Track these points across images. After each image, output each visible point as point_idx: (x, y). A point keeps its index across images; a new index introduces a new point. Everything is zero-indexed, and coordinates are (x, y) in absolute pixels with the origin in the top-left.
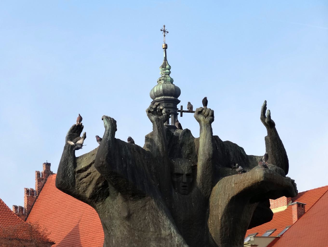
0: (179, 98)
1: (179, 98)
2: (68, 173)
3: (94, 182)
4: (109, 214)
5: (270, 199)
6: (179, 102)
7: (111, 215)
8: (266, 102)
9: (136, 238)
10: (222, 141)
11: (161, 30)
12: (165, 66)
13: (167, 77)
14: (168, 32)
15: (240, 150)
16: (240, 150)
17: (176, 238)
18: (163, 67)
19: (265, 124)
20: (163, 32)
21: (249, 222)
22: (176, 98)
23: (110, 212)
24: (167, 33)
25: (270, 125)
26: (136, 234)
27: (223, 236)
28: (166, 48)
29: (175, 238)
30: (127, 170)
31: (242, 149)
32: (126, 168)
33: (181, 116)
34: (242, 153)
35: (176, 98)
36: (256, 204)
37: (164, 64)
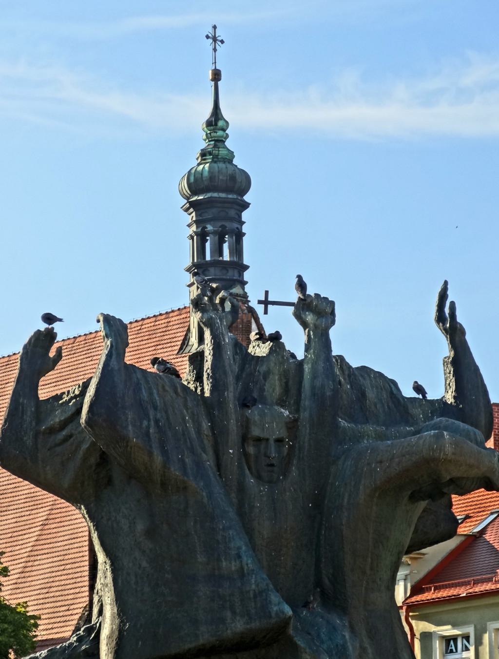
0: (247, 198)
1: (247, 198)
2: (23, 433)
3: (80, 454)
4: (110, 523)
5: (453, 496)
6: (246, 205)
7: (115, 525)
8: (446, 283)
9: (166, 575)
10: (350, 367)
11: (208, 37)
12: (216, 121)
13: (219, 148)
14: (222, 42)
15: (389, 387)
16: (390, 386)
17: (252, 577)
18: (209, 124)
19: (446, 331)
20: (211, 41)
21: (407, 543)
22: (239, 198)
23: (113, 519)
24: (220, 43)
25: (455, 333)
26: (166, 567)
27: (370, 651)
28: (217, 76)
29: (250, 578)
30: (151, 431)
31: (394, 383)
32: (148, 427)
33: (266, 312)
34: (395, 392)
35: (239, 198)
36: (423, 504)
37: (212, 115)
